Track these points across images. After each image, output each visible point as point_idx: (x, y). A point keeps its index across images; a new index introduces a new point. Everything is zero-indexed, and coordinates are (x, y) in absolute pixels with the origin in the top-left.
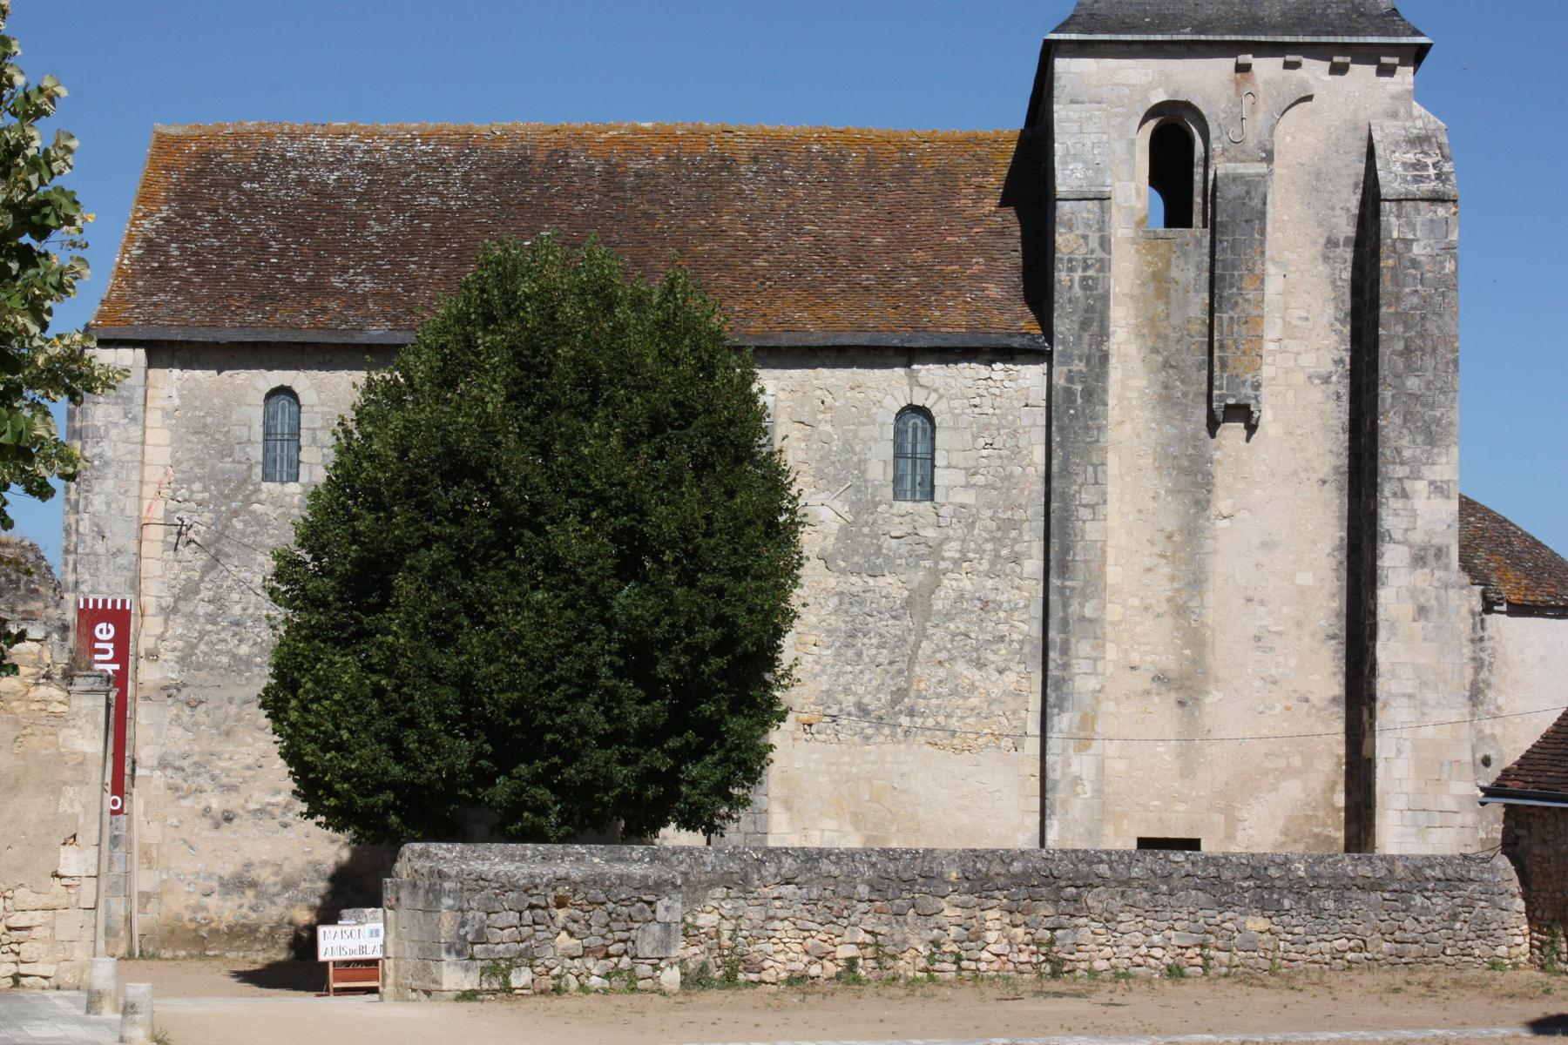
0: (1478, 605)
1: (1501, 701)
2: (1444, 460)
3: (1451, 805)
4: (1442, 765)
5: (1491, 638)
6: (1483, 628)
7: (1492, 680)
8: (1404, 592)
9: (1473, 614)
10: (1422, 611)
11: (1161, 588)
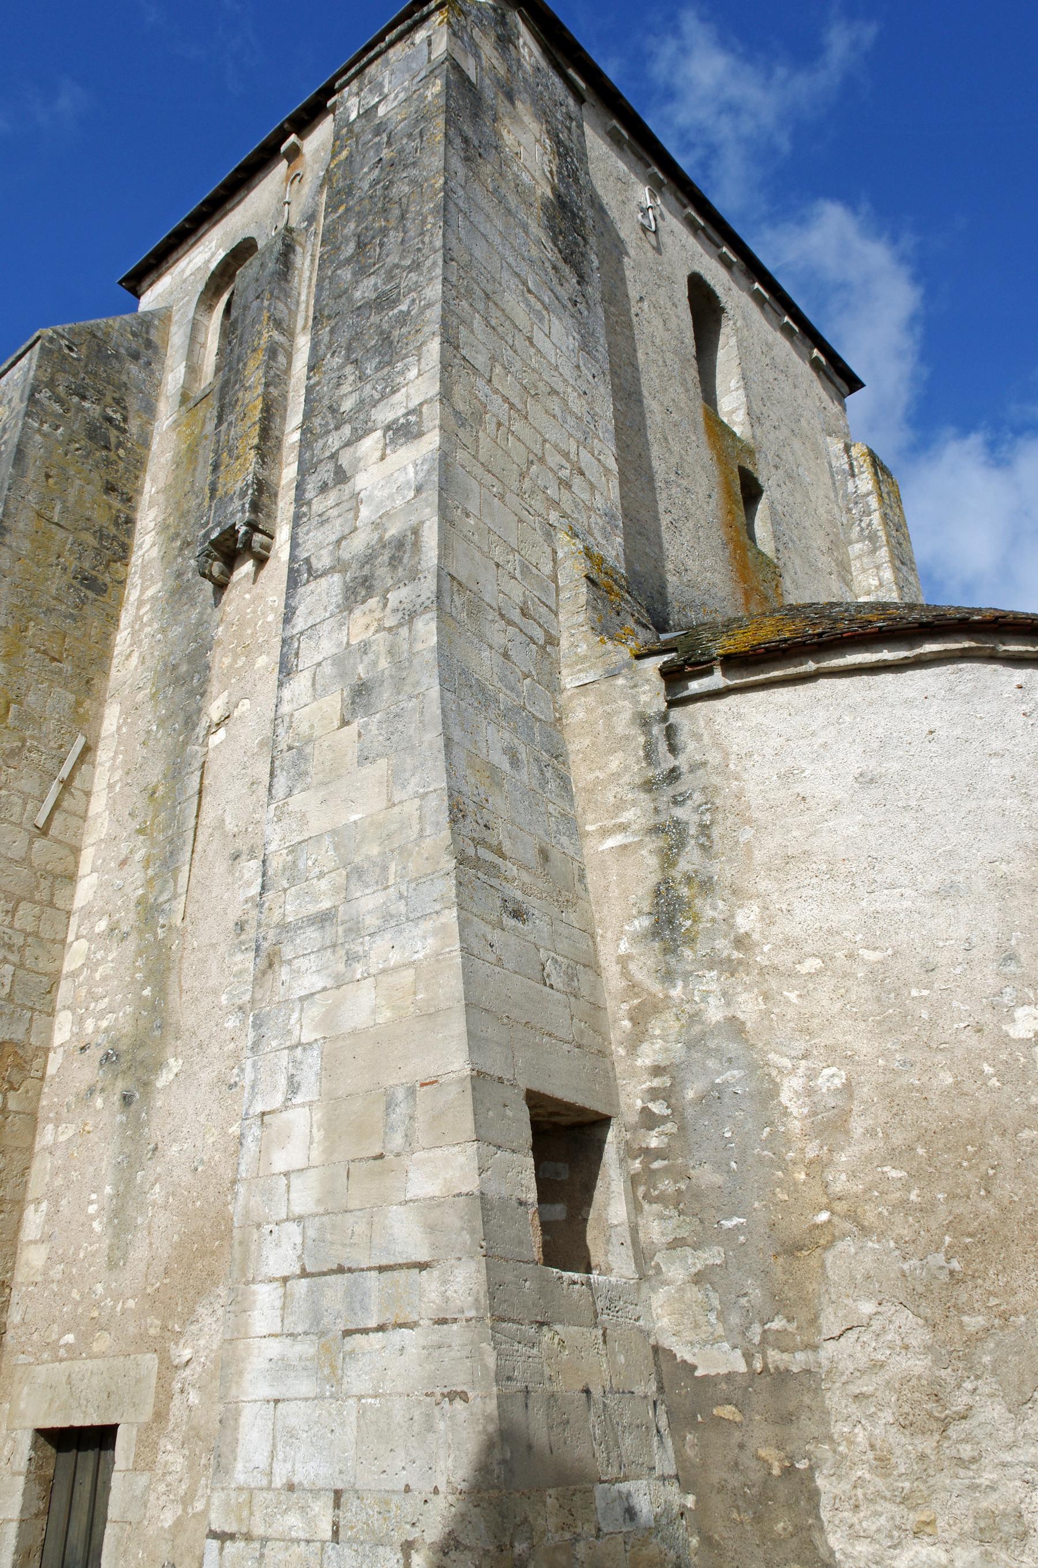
0: (651, 693)
1: (746, 920)
2: (413, 373)
3: (407, 1238)
4: (390, 1105)
5: (693, 768)
6: (673, 749)
7: (715, 868)
8: (328, 669)
9: (644, 722)
10: (361, 694)
11: (134, 881)
